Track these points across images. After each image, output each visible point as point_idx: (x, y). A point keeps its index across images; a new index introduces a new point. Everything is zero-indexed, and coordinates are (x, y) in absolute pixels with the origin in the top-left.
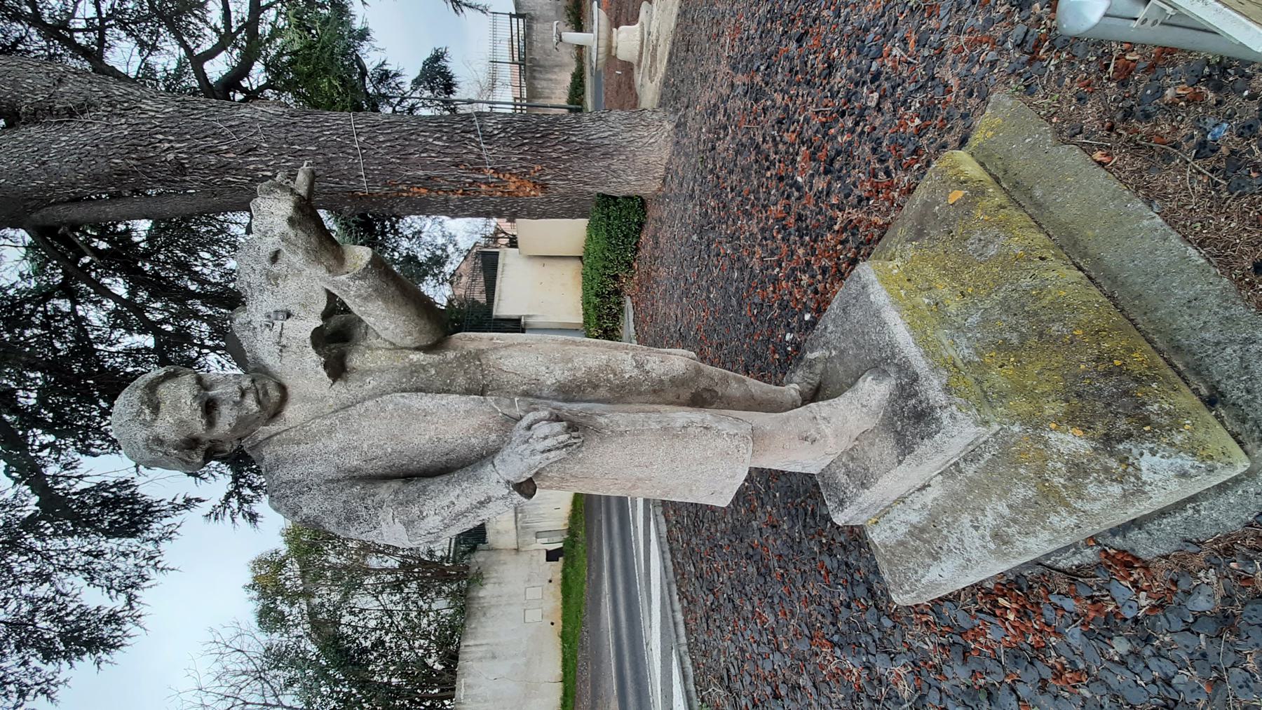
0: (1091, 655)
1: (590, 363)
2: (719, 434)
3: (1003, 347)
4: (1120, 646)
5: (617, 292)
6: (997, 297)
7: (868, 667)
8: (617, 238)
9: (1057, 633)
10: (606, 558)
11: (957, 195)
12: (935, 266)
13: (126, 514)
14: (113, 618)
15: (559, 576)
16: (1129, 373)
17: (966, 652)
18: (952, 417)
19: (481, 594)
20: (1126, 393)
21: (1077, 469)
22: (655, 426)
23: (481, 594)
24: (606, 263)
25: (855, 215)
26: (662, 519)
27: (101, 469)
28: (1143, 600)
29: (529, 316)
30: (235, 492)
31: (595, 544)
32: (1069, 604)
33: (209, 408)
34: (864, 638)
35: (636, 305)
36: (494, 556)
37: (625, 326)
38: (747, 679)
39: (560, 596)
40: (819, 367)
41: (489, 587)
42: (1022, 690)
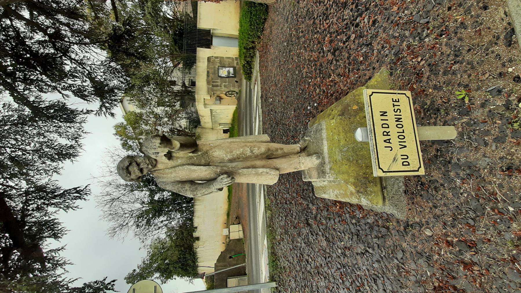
0: (349, 220)
1: (238, 153)
2: (270, 174)
3: (348, 160)
4: (354, 221)
5: (253, 48)
6: (353, 146)
7: (308, 205)
8: (254, 26)
9: (345, 214)
11: (355, 107)
13: (64, 114)
14: (72, 147)
16: (368, 179)
17: (328, 210)
18: (329, 177)
20: (365, 184)
21: (352, 194)
22: (253, 172)
24: (249, 37)
25: (337, 79)
27: (50, 97)
28: (361, 216)
29: (214, 29)
32: (348, 210)
33: (141, 170)
34: (308, 199)
35: (261, 57)
36: (204, 130)
37: (255, 66)
38: (280, 197)
40: (307, 142)
42: (336, 221)
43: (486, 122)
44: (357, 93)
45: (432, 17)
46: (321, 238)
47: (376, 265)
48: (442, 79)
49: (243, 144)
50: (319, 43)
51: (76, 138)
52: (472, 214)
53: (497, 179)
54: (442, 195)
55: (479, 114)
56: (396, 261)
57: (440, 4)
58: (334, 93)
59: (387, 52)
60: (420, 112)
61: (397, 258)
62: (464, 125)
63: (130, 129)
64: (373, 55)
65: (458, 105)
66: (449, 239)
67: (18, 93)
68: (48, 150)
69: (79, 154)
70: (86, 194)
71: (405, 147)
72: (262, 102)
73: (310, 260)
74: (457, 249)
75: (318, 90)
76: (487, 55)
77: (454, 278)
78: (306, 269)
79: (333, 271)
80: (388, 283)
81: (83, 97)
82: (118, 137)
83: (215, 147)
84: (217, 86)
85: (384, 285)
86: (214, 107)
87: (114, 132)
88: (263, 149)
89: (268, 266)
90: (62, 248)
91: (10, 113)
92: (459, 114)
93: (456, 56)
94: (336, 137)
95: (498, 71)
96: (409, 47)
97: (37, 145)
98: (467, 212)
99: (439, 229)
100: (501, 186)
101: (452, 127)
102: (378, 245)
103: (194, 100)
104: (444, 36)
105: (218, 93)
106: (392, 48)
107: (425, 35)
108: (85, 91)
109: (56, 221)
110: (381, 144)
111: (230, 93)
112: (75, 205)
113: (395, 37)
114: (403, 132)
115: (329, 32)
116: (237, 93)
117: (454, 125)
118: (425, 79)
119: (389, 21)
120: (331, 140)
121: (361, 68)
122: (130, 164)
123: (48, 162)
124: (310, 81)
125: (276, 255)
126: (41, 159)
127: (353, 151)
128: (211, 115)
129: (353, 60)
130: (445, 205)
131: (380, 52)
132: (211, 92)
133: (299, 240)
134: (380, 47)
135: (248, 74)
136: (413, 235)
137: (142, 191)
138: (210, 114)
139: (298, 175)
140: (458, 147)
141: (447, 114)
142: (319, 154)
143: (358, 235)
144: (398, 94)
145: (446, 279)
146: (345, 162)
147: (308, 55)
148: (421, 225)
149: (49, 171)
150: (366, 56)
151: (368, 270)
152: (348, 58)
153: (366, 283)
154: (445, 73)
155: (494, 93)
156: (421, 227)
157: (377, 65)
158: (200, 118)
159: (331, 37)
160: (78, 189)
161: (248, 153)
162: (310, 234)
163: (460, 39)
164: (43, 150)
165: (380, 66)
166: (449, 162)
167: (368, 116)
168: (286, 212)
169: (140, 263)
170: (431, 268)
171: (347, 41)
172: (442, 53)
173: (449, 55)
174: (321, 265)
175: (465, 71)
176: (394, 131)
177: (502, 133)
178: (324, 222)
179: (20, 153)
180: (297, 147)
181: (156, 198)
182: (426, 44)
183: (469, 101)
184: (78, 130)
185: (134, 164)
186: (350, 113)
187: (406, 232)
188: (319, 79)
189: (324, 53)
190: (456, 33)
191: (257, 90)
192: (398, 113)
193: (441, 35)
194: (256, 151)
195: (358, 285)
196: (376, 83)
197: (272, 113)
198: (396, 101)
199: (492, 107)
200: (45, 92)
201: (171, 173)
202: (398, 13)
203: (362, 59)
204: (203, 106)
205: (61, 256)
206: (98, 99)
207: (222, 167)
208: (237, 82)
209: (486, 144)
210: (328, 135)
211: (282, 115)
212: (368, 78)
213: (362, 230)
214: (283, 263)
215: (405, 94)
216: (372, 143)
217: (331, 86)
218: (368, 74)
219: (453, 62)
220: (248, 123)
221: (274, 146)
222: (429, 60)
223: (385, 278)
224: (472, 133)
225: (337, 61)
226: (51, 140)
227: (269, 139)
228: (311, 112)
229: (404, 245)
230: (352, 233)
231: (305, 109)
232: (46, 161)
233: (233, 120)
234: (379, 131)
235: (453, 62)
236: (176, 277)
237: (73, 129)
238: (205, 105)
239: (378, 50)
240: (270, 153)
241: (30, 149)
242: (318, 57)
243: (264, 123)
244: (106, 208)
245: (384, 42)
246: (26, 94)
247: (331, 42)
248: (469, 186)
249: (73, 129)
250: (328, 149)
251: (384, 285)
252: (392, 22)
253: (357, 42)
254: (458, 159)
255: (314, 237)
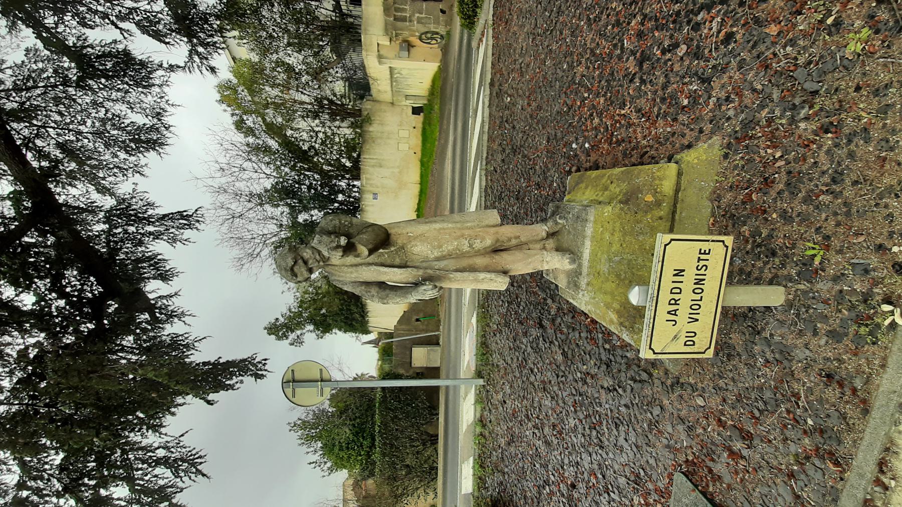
3: (618, 276)
7: (545, 299)
10: (451, 138)
11: (649, 198)
12: (621, 224)
13: (128, 69)
14: (153, 128)
15: (420, 125)
19: (371, 129)
20: (634, 317)
23: (371, 129)
26: (484, 178)
30: (192, 52)
31: (445, 122)
36: (377, 106)
39: (421, 138)
41: (375, 125)
43: (829, 304)
44: (658, 174)
45: (826, 87)
46: (555, 348)
47: (623, 409)
48: (799, 207)
49: (459, 233)
50: (618, 23)
51: (159, 114)
52: (761, 405)
53: (811, 380)
54: (734, 366)
55: (825, 288)
56: (649, 415)
57: (847, 69)
58: (623, 141)
59: (731, 113)
60: (747, 241)
61: (651, 413)
62: (799, 293)
63: (244, 93)
64: (707, 106)
65: (804, 261)
66: (723, 418)
67: (48, 30)
68: (115, 132)
69: (169, 141)
70: (198, 221)
71: (697, 320)
72: (491, 94)
73: (536, 370)
74: (728, 433)
75: (596, 120)
76: (877, 205)
77: (713, 460)
78: (528, 379)
79: (565, 394)
80: (632, 434)
81: (158, 36)
82: (224, 106)
83: (415, 238)
84: (404, 19)
85: (627, 433)
86: (398, 64)
87: (218, 97)
88: (488, 242)
89: (474, 358)
90: (176, 294)
91: (40, 65)
92: (798, 274)
93: (834, 181)
94: (607, 236)
95: (879, 241)
96: (770, 121)
97: (97, 124)
98: (756, 400)
99: (715, 402)
100: (810, 391)
101: (782, 289)
102: (632, 389)
103: (356, 42)
104: (830, 135)
105: (406, 34)
106: (742, 108)
107: (802, 115)
108: (159, 22)
109: (159, 257)
110: (664, 307)
111: (429, 35)
112: (185, 237)
113: (754, 90)
114: (701, 300)
115: (641, 10)
116: (442, 37)
117: (785, 286)
118: (773, 194)
119: (755, 53)
120: (597, 240)
121: (681, 117)
122: (295, 263)
123: (122, 155)
124: (586, 95)
125: (487, 347)
126: (108, 149)
127: (629, 265)
128: (392, 77)
129: (671, 97)
130: (733, 379)
131: (720, 106)
132: (391, 31)
133: (524, 341)
134: (723, 95)
135: (469, 17)
136: (681, 396)
137: (278, 206)
138: (389, 77)
139: (538, 277)
140: (778, 320)
141: (784, 265)
142: (573, 253)
143: (608, 366)
144: (713, 241)
145: (703, 457)
146: (612, 277)
147: (593, 40)
148: (694, 388)
149: (127, 170)
150: (694, 98)
151: (611, 411)
152: (664, 87)
153: (605, 423)
154: (807, 200)
155: (859, 270)
156: (694, 392)
157: (708, 127)
158: (371, 82)
159: (642, 24)
160: (185, 214)
161: (466, 248)
162: (541, 339)
163: (851, 155)
164: (109, 132)
165: (713, 133)
166: (759, 333)
167: (654, 277)
168: (511, 297)
169: (285, 310)
170: (689, 440)
171: (669, 51)
172: (815, 163)
173: (824, 173)
174: (550, 382)
175: (836, 214)
176: (686, 298)
177: (842, 329)
178: (565, 330)
179: (73, 138)
180: (542, 229)
181: (301, 218)
182: (798, 132)
183: (820, 264)
184: (159, 100)
185: (300, 262)
186: (639, 205)
187: (673, 389)
188: (602, 100)
189: (622, 52)
190: (850, 141)
191: (483, 53)
192: (702, 272)
193: (827, 131)
194: (478, 245)
195: (595, 421)
196: (696, 161)
197: (507, 126)
198: (705, 253)
199: (845, 288)
200: (91, 27)
201: (351, 273)
202: (774, 43)
203: (686, 102)
204: (376, 60)
205: (176, 304)
206: (185, 39)
207: (426, 268)
208: (443, 12)
209: (815, 333)
210: (595, 231)
211: (525, 138)
212: (687, 143)
213: (616, 362)
214: (496, 358)
215: (723, 242)
216: (648, 314)
217: (622, 126)
218: (689, 136)
219: (824, 189)
220: (461, 106)
221: (509, 231)
222: (793, 164)
223: (631, 429)
224: (804, 310)
225: (643, 82)
226: (118, 116)
227: (499, 220)
228: (576, 155)
229: (666, 402)
230: (601, 360)
231: (568, 144)
232: (119, 153)
233: (432, 92)
234: (665, 296)
235: (824, 189)
236: (337, 331)
237: (150, 97)
238: (380, 57)
239: (718, 99)
240: (498, 244)
241: (86, 130)
242: (610, 55)
243: (491, 139)
244: (224, 229)
245: (733, 89)
246: (61, 33)
247: (640, 35)
248: (772, 372)
249: (150, 97)
250: (591, 254)
251: (627, 433)
252: (758, 57)
253: (687, 63)
254: (771, 335)
255: (547, 345)
